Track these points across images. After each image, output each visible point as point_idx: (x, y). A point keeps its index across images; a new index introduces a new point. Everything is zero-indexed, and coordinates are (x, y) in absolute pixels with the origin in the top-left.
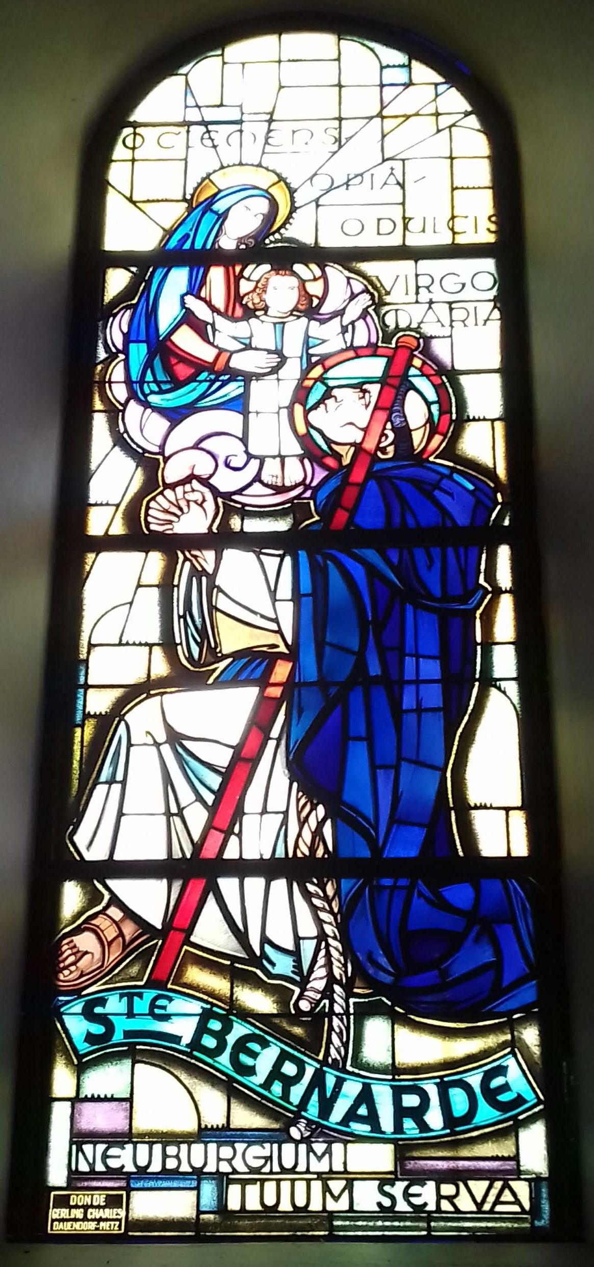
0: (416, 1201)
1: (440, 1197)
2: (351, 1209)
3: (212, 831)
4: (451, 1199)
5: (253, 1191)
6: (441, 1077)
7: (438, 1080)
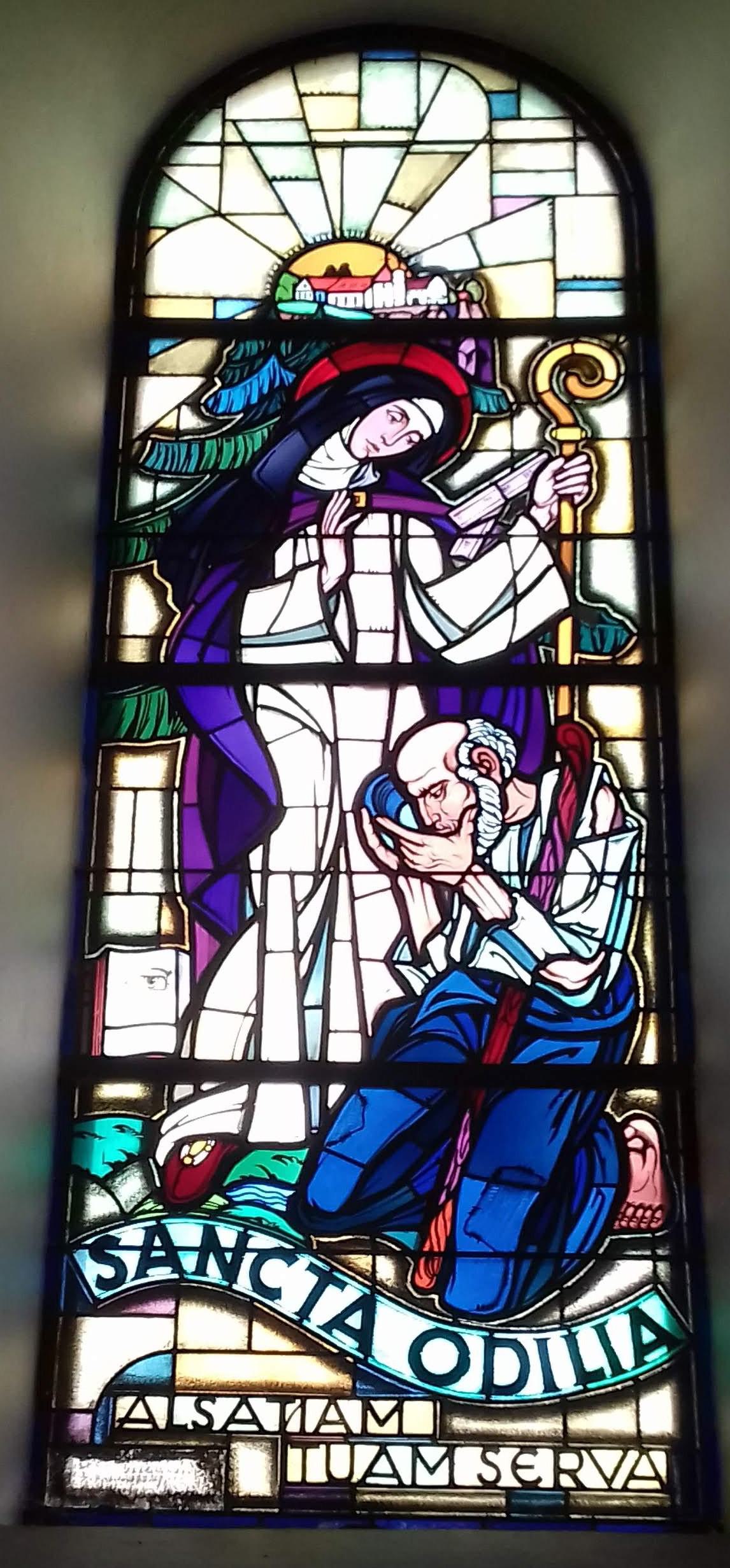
0: (527, 1475)
1: (558, 1471)
2: (452, 1484)
3: (307, 1012)
4: (572, 1473)
5: (316, 1456)
6: (491, 1332)
7: (487, 1334)
